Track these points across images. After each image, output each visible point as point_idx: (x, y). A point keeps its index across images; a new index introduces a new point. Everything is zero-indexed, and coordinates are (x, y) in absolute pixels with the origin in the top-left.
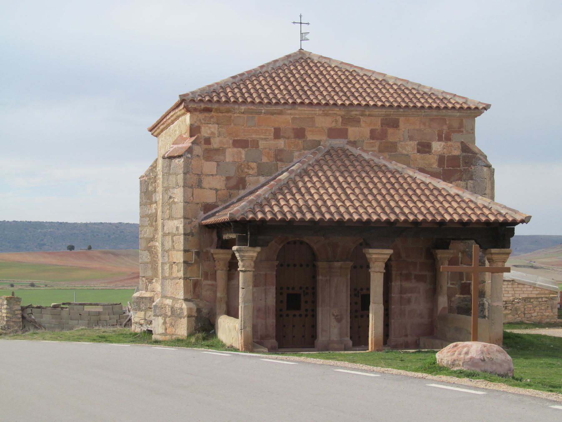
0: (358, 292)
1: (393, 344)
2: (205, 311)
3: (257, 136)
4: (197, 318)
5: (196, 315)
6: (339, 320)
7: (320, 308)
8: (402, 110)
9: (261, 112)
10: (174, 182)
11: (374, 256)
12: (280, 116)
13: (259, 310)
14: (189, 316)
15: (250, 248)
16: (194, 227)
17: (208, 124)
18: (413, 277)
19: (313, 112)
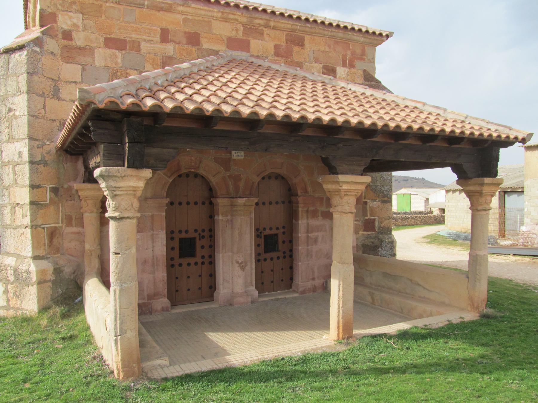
0: (261, 233)
1: (301, 290)
2: (67, 270)
3: (139, 37)
4: (54, 282)
5: (53, 278)
6: (243, 268)
7: (221, 255)
8: (309, 25)
9: (144, 5)
10: (14, 87)
11: (345, 187)
12: (169, 14)
13: (145, 262)
14: (40, 283)
15: (131, 171)
16: (47, 153)
17: (67, 11)
18: (320, 215)
19: (210, 14)
